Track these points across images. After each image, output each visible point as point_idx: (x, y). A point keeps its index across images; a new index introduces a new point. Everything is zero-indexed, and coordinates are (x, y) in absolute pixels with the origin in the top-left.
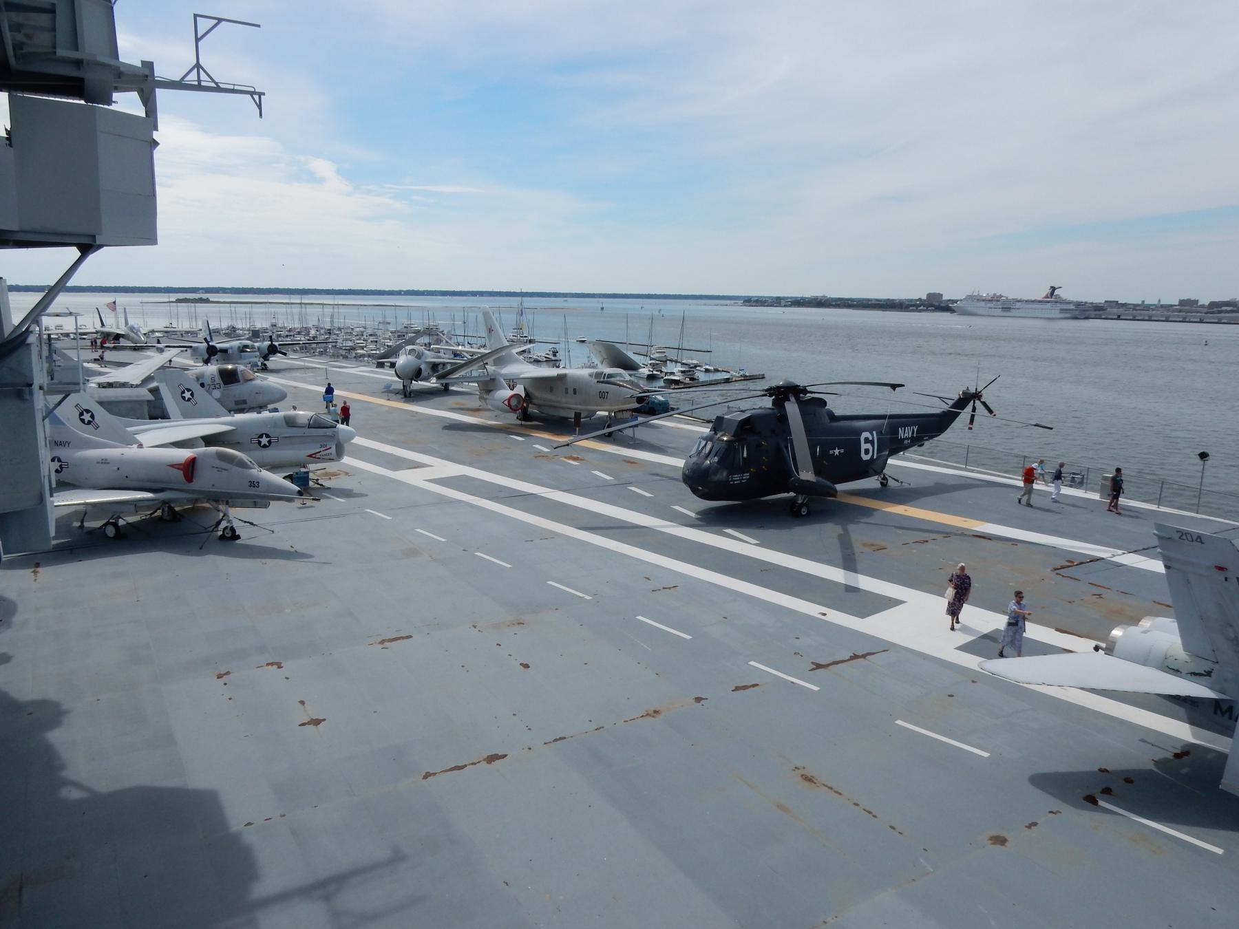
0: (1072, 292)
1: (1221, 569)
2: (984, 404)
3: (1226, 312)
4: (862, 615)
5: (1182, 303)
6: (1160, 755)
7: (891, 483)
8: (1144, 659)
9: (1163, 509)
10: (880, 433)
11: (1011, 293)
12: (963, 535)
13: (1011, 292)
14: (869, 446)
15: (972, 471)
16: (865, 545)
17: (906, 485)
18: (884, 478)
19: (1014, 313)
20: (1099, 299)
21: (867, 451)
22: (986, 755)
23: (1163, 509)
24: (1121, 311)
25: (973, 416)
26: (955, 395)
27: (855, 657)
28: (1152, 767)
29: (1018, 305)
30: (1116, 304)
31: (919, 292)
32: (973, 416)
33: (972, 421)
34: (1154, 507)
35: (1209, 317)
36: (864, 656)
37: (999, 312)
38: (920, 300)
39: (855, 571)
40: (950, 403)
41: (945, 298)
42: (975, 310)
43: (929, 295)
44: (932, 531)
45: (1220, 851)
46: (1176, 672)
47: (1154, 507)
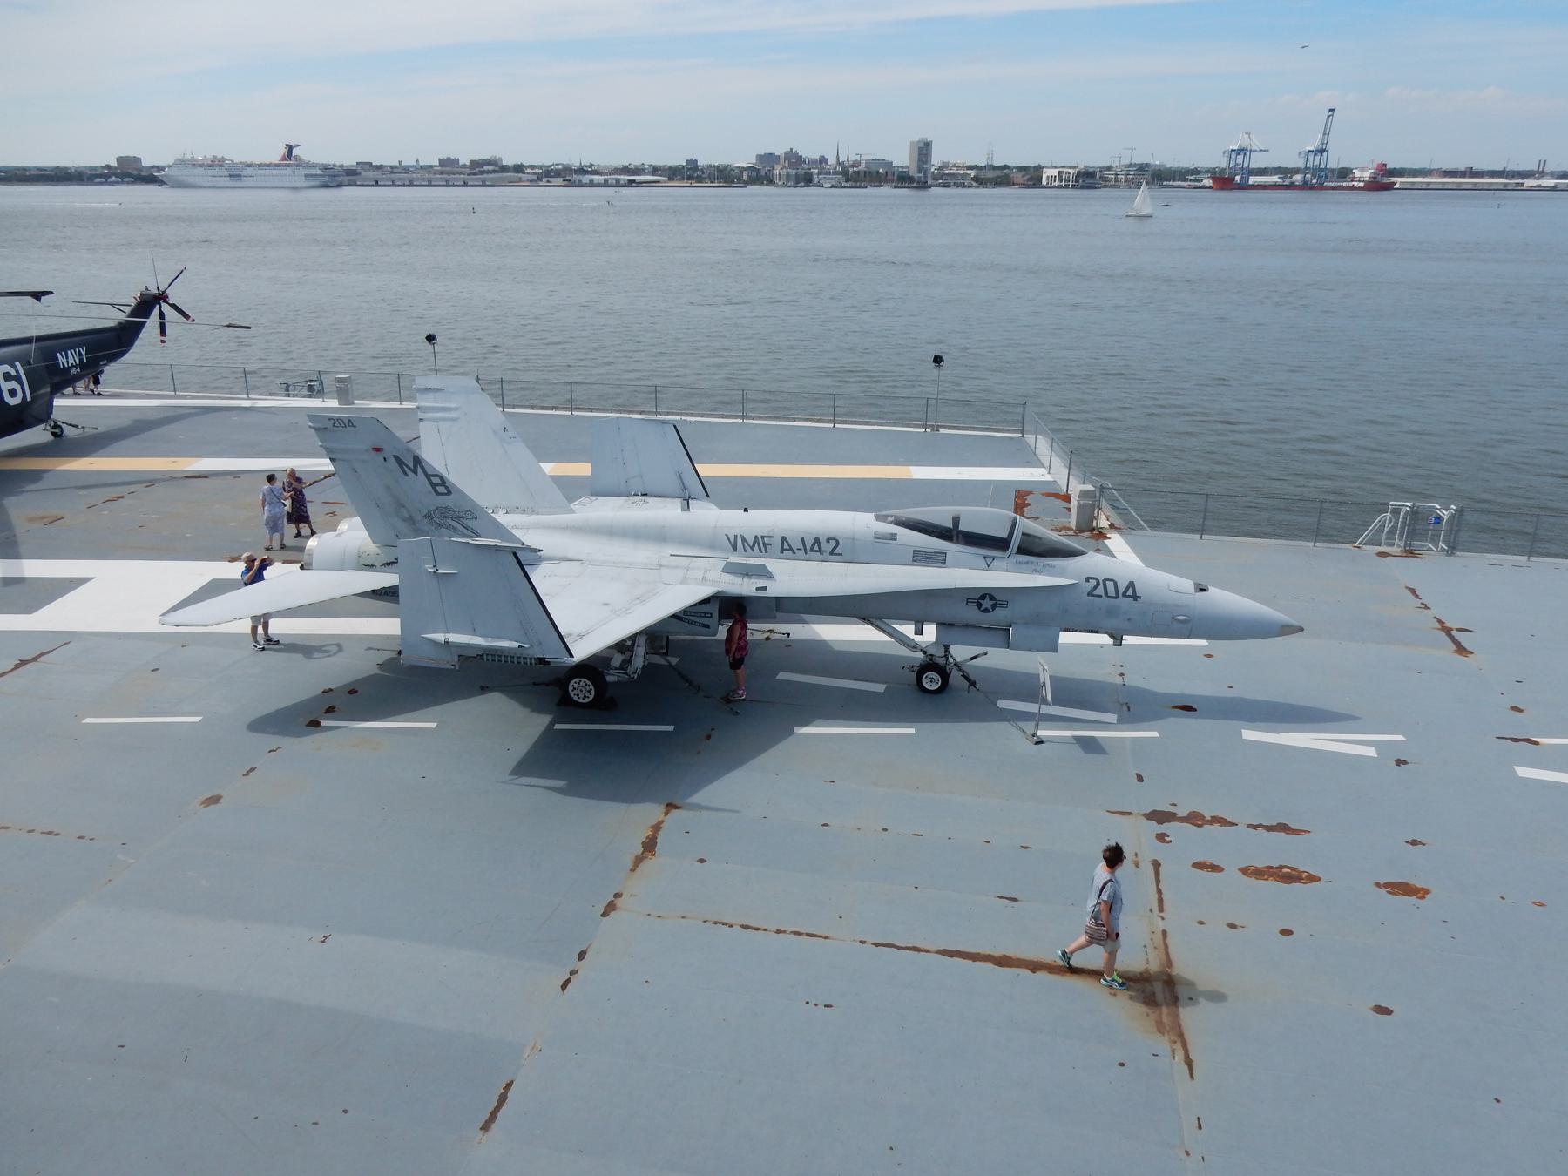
0: (319, 151)
1: (378, 450)
2: (174, 306)
3: (489, 172)
4: (30, 610)
5: (443, 162)
6: (383, 657)
7: (68, 431)
8: (341, 564)
9: (406, 405)
10: (26, 363)
11: (237, 155)
12: (172, 478)
13: (237, 154)
14: (13, 384)
15: (185, 397)
16: (32, 520)
17: (90, 431)
18: (56, 426)
19: (247, 182)
20: (349, 160)
21: (13, 393)
22: (197, 719)
23: (406, 405)
24: (377, 175)
25: (162, 326)
26: (131, 298)
27: (23, 663)
28: (377, 671)
29: (250, 170)
30: (370, 166)
31: (105, 157)
32: (162, 326)
33: (163, 332)
34: (396, 405)
35: (472, 180)
36: (35, 659)
37: (227, 182)
38: (108, 167)
39: (17, 556)
40: (128, 310)
41: (145, 163)
42: (191, 180)
43: (120, 160)
44: (124, 484)
45: (433, 725)
46: (371, 567)
47: (396, 405)
